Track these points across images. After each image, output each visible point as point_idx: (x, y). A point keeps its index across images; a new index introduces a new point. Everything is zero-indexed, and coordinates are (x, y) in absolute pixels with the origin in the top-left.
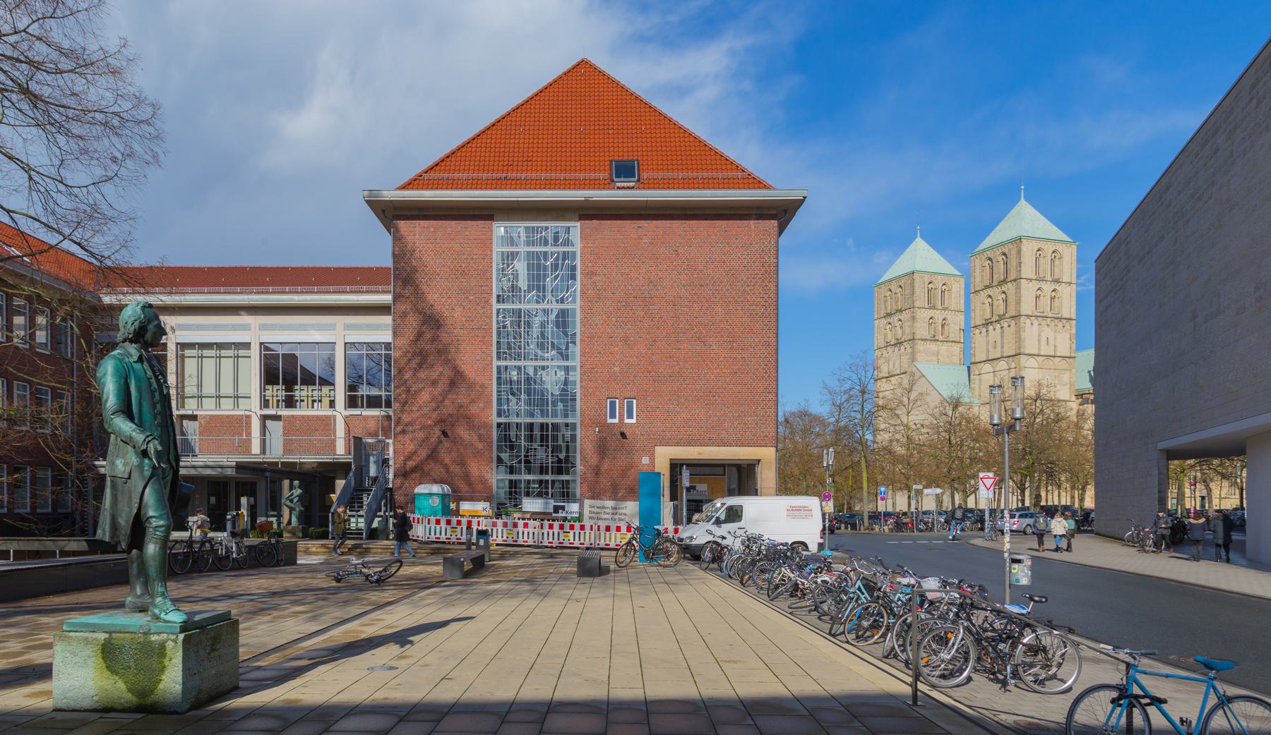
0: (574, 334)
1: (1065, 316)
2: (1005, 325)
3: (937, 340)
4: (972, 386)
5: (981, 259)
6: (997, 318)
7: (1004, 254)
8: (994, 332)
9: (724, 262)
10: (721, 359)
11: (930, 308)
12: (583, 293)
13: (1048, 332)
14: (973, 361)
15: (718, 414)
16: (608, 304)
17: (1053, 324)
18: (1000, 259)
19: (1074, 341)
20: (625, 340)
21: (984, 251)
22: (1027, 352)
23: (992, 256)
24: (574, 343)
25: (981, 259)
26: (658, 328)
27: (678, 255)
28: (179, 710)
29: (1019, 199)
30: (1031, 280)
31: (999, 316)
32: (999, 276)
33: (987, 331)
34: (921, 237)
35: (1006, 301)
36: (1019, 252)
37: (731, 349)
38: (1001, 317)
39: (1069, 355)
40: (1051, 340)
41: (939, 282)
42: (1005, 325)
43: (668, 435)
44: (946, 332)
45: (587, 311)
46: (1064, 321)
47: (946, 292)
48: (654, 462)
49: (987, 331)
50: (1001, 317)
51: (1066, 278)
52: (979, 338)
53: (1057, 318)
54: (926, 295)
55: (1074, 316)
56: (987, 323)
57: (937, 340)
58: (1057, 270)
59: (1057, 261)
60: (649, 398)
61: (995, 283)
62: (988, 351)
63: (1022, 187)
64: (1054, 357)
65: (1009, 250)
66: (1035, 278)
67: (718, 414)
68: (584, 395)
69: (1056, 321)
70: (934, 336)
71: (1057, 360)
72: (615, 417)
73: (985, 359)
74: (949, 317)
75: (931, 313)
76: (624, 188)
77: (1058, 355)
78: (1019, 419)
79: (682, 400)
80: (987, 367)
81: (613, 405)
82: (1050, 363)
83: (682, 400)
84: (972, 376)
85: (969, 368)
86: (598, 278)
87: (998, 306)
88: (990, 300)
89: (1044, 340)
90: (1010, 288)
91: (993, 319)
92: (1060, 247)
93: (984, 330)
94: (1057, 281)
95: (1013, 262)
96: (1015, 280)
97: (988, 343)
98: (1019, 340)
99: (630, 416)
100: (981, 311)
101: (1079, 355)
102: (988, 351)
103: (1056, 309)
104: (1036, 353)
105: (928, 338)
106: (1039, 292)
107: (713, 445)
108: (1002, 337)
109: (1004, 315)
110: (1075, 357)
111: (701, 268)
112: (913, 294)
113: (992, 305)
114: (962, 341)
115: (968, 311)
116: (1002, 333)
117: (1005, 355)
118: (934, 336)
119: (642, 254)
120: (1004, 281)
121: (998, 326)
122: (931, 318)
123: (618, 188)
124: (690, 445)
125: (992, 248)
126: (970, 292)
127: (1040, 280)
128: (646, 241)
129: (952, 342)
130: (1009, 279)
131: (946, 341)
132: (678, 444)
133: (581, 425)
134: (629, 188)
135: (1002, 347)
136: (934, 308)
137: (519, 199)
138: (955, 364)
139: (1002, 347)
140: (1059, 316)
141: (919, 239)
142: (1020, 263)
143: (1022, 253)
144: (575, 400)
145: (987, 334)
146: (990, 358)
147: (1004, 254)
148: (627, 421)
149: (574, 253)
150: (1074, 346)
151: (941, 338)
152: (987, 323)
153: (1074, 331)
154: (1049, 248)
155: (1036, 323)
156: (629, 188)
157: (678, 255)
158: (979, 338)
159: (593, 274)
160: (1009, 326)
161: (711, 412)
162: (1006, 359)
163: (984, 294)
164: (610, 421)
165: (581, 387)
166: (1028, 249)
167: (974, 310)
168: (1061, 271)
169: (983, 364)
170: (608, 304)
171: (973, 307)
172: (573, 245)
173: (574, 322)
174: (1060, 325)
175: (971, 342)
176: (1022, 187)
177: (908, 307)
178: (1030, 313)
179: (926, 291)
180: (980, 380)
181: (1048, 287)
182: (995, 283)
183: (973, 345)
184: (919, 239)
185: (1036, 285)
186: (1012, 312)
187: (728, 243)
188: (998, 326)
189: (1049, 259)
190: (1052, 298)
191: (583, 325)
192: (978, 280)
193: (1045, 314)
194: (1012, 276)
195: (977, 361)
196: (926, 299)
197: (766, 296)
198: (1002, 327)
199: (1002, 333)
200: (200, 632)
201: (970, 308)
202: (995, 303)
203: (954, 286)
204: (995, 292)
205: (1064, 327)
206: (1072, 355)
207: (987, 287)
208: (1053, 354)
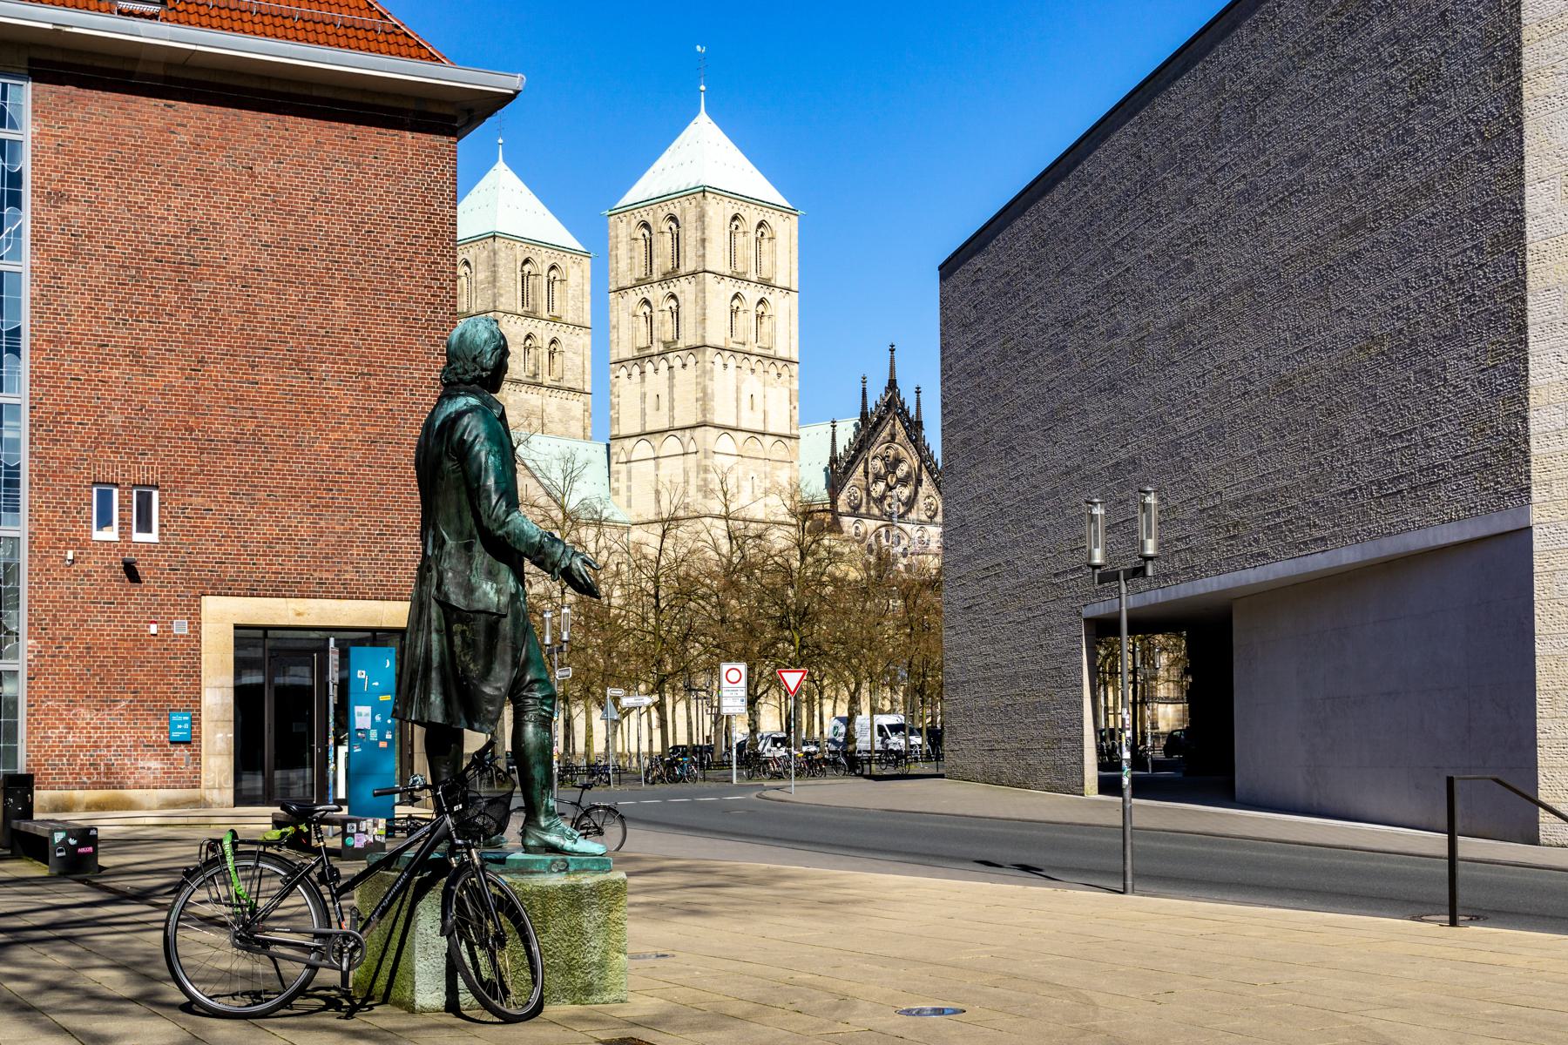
0: (16, 332)
1: (782, 354)
2: (677, 363)
3: (541, 385)
4: (615, 485)
5: (629, 223)
6: (661, 348)
7: (673, 218)
8: (656, 379)
9: (351, 204)
10: (346, 411)
11: (526, 315)
12: (37, 241)
13: (752, 384)
14: (615, 432)
15: (339, 529)
16: (97, 270)
17: (759, 368)
18: (665, 228)
19: (797, 404)
20: (136, 355)
21: (635, 206)
22: (717, 421)
23: (650, 220)
24: (16, 351)
25: (629, 223)
26: (210, 334)
27: (253, 176)
28: (736, 1009)
29: (696, 113)
30: (723, 276)
31: (664, 343)
32: (662, 263)
33: (642, 373)
34: (505, 160)
35: (676, 314)
36: (701, 217)
37: (365, 389)
38: (669, 347)
39: (787, 432)
40: (758, 399)
41: (543, 260)
42: (677, 363)
43: (232, 571)
44: (557, 367)
45: (49, 284)
46: (780, 364)
47: (557, 284)
48: (199, 632)
49: (642, 373)
50: (669, 347)
51: (781, 281)
52: (627, 388)
53: (768, 357)
54: (520, 287)
55: (795, 357)
56: (642, 357)
57: (541, 385)
58: (766, 262)
59: (765, 242)
60: (190, 488)
61: (656, 276)
62: (644, 413)
63: (703, 88)
64: (764, 434)
65: (683, 210)
66: (728, 272)
67: (339, 529)
68: (39, 475)
69: (767, 362)
70: (535, 375)
71: (769, 440)
72: (149, 531)
73: (638, 430)
74: (562, 337)
75: (528, 326)
76: (131, 14)
77: (771, 430)
78: (1151, 558)
79: (262, 495)
80: (643, 449)
81: (105, 499)
82: (753, 447)
83: (262, 495)
84: (614, 467)
85: (608, 446)
86: (74, 209)
87: (663, 324)
88: (646, 309)
89: (651, 400)
90: (683, 288)
91: (654, 350)
92: (773, 219)
93: (636, 370)
94: (766, 283)
95: (690, 236)
96: (694, 274)
97: (644, 396)
98: (704, 399)
99: (145, 525)
100: (628, 335)
101: (802, 432)
102: (644, 413)
103: (766, 338)
104: (733, 424)
105: (524, 379)
106: (736, 303)
107: (328, 594)
108: (671, 387)
109: (675, 342)
110: (797, 438)
111: (302, 210)
112: (494, 281)
113: (650, 320)
114: (588, 389)
115: (600, 328)
116: (671, 378)
117: (677, 424)
118: (535, 375)
119: (176, 166)
120: (671, 276)
121: (663, 365)
122: (528, 337)
123: (120, 12)
124: (277, 594)
125: (648, 202)
126: (603, 290)
127: (737, 277)
128: (185, 138)
129: (570, 390)
130: (682, 270)
131: (559, 388)
132: (252, 593)
133: (31, 543)
134: (142, 15)
135: (672, 408)
136: (531, 315)
137: (199, 48)
138: (574, 437)
139: (672, 408)
140: (771, 353)
141: (501, 166)
142: (703, 240)
143: (707, 219)
144: (17, 484)
145: (643, 380)
146: (648, 429)
147: (673, 218)
148: (138, 537)
149: (16, 144)
150: (796, 418)
151: (547, 381)
152: (642, 357)
153: (796, 385)
154: (752, 216)
155: (732, 363)
156: (142, 15)
157: (253, 176)
158: (627, 388)
159: (59, 197)
160: (684, 366)
161: (322, 523)
162: (678, 434)
163: (634, 297)
164: (98, 535)
165: (31, 454)
166: (718, 212)
167: (616, 327)
168: (774, 264)
169: (634, 440)
170: (97, 270)
171: (614, 321)
172: (13, 126)
173: (18, 302)
174: (773, 371)
175: (611, 393)
176: (703, 88)
177: (483, 308)
178: (721, 344)
179: (519, 279)
180: (629, 472)
181: (752, 294)
182: (656, 276)
183: (615, 400)
184: (501, 166)
185: (729, 287)
186: (688, 338)
187: (358, 165)
188: (663, 365)
189: (752, 236)
190: (760, 317)
191: (37, 312)
192: (623, 265)
193: (747, 348)
194: (689, 265)
195: (623, 433)
196: (520, 294)
197: (435, 284)
198: (670, 368)
199: (671, 378)
200: (256, 933)
201: (607, 320)
202: (657, 316)
203: (571, 272)
204: (656, 294)
205: (779, 375)
206: (794, 432)
207: (640, 283)
208: (760, 428)
